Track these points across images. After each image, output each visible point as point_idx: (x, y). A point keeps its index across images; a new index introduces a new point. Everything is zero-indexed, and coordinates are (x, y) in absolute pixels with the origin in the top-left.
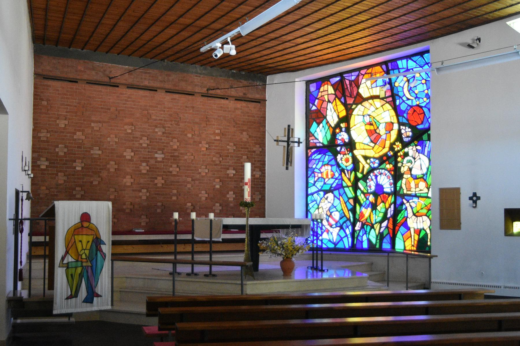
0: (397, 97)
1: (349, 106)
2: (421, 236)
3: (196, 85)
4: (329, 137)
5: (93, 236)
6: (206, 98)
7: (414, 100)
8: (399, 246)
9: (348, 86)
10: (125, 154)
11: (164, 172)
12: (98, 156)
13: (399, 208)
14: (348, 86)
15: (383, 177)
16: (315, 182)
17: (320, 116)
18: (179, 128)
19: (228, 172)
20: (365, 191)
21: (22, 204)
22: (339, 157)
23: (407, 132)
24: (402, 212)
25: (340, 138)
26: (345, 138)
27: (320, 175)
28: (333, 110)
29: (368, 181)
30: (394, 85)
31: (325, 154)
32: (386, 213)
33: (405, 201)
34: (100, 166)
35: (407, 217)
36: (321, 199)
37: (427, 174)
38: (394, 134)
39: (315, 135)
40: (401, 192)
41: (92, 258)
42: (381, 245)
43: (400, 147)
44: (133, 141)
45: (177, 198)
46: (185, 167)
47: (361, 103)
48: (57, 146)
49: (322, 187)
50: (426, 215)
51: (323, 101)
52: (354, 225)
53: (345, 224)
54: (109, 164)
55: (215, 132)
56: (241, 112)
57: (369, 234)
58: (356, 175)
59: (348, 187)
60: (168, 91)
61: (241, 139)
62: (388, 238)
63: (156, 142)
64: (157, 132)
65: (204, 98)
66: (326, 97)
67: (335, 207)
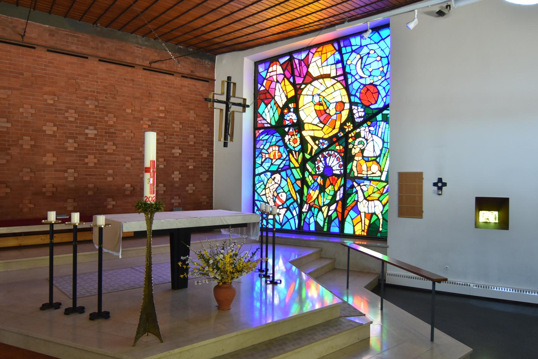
0: (349, 76)
2: (372, 221)
4: (277, 118)
6: (148, 72)
8: (348, 229)
9: (298, 65)
10: (44, 128)
11: (97, 150)
12: (5, 130)
13: (349, 192)
14: (298, 65)
16: (262, 163)
17: (268, 96)
19: (173, 151)
20: (313, 173)
22: (287, 138)
23: (359, 113)
24: (352, 196)
25: (288, 119)
26: (293, 118)
27: (267, 156)
28: (281, 91)
29: (316, 163)
30: (346, 64)
31: (272, 135)
32: (334, 196)
33: (355, 184)
34: (9, 141)
35: (358, 201)
36: (268, 180)
37: (380, 156)
38: (345, 114)
39: (264, 115)
42: (329, 228)
43: (352, 128)
44: (56, 113)
45: (113, 179)
47: (310, 83)
49: (270, 167)
50: (378, 200)
51: (272, 81)
52: (301, 207)
53: (292, 205)
56: (188, 90)
58: (304, 155)
59: (295, 168)
61: (188, 118)
62: (337, 221)
63: (87, 116)
64: (88, 105)
65: (145, 71)
66: (275, 77)
67: (282, 188)
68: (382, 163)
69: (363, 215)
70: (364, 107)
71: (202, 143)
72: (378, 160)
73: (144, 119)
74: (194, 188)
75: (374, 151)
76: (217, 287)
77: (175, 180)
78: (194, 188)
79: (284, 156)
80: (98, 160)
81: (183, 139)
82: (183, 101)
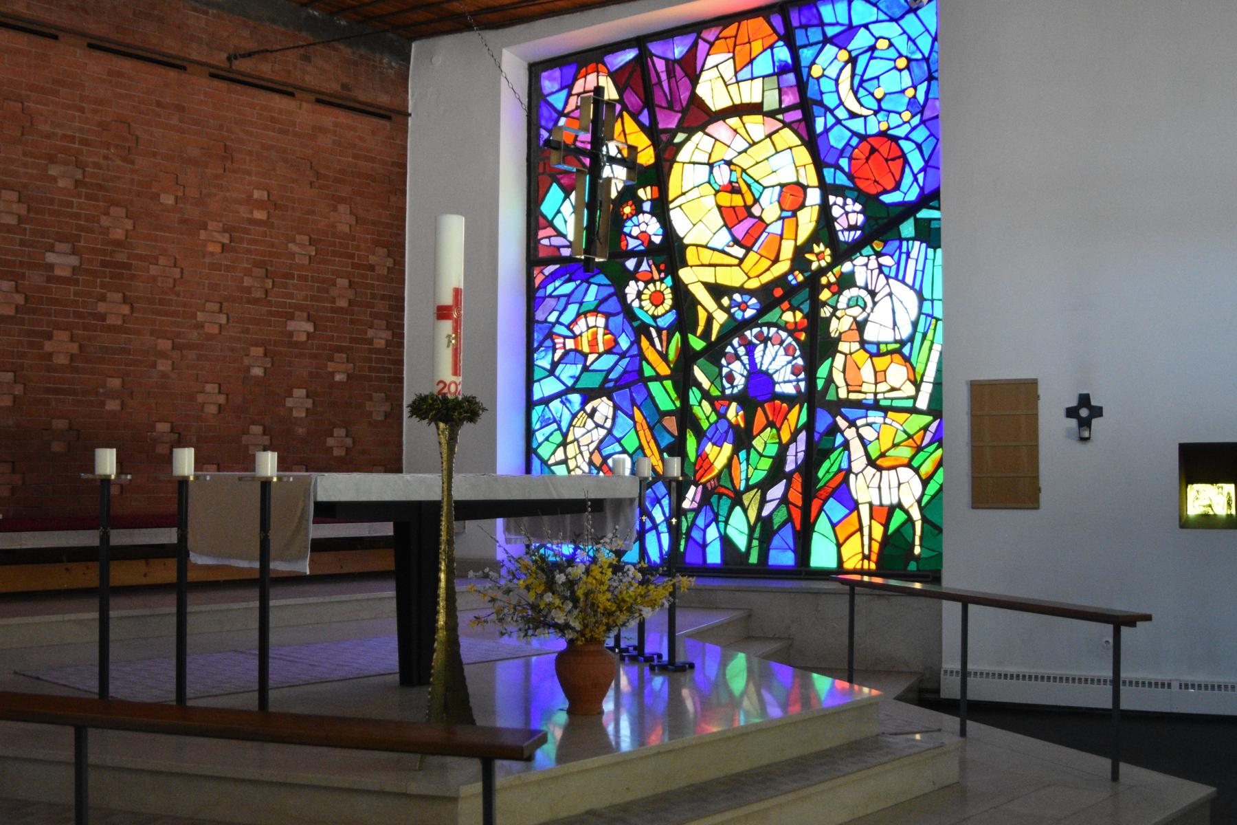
0: (817, 110)
1: (664, 137)
2: (893, 527)
6: (223, 85)
7: (872, 120)
8: (822, 555)
9: (664, 76)
11: (77, 315)
13: (825, 444)
14: (664, 76)
15: (771, 349)
16: (555, 365)
19: (292, 326)
20: (715, 392)
22: (632, 289)
23: (849, 215)
24: (833, 457)
25: (635, 232)
29: (724, 362)
30: (809, 75)
32: (780, 459)
36: (574, 416)
37: (911, 339)
38: (807, 220)
39: (558, 222)
40: (831, 396)
42: (764, 555)
43: (828, 259)
45: (123, 405)
47: (702, 128)
50: (909, 465)
55: (250, 196)
57: (726, 523)
58: (685, 341)
59: (658, 378)
60: (97, 46)
62: (787, 533)
64: (54, 179)
65: (216, 83)
67: (619, 440)
68: (918, 361)
69: (864, 511)
70: (863, 199)
71: (369, 305)
72: (906, 350)
73: (212, 225)
74: (349, 441)
75: (895, 324)
76: (562, 658)
77: (295, 414)
78: (349, 441)
79: (624, 342)
80: (81, 347)
81: (319, 290)
82: (318, 176)
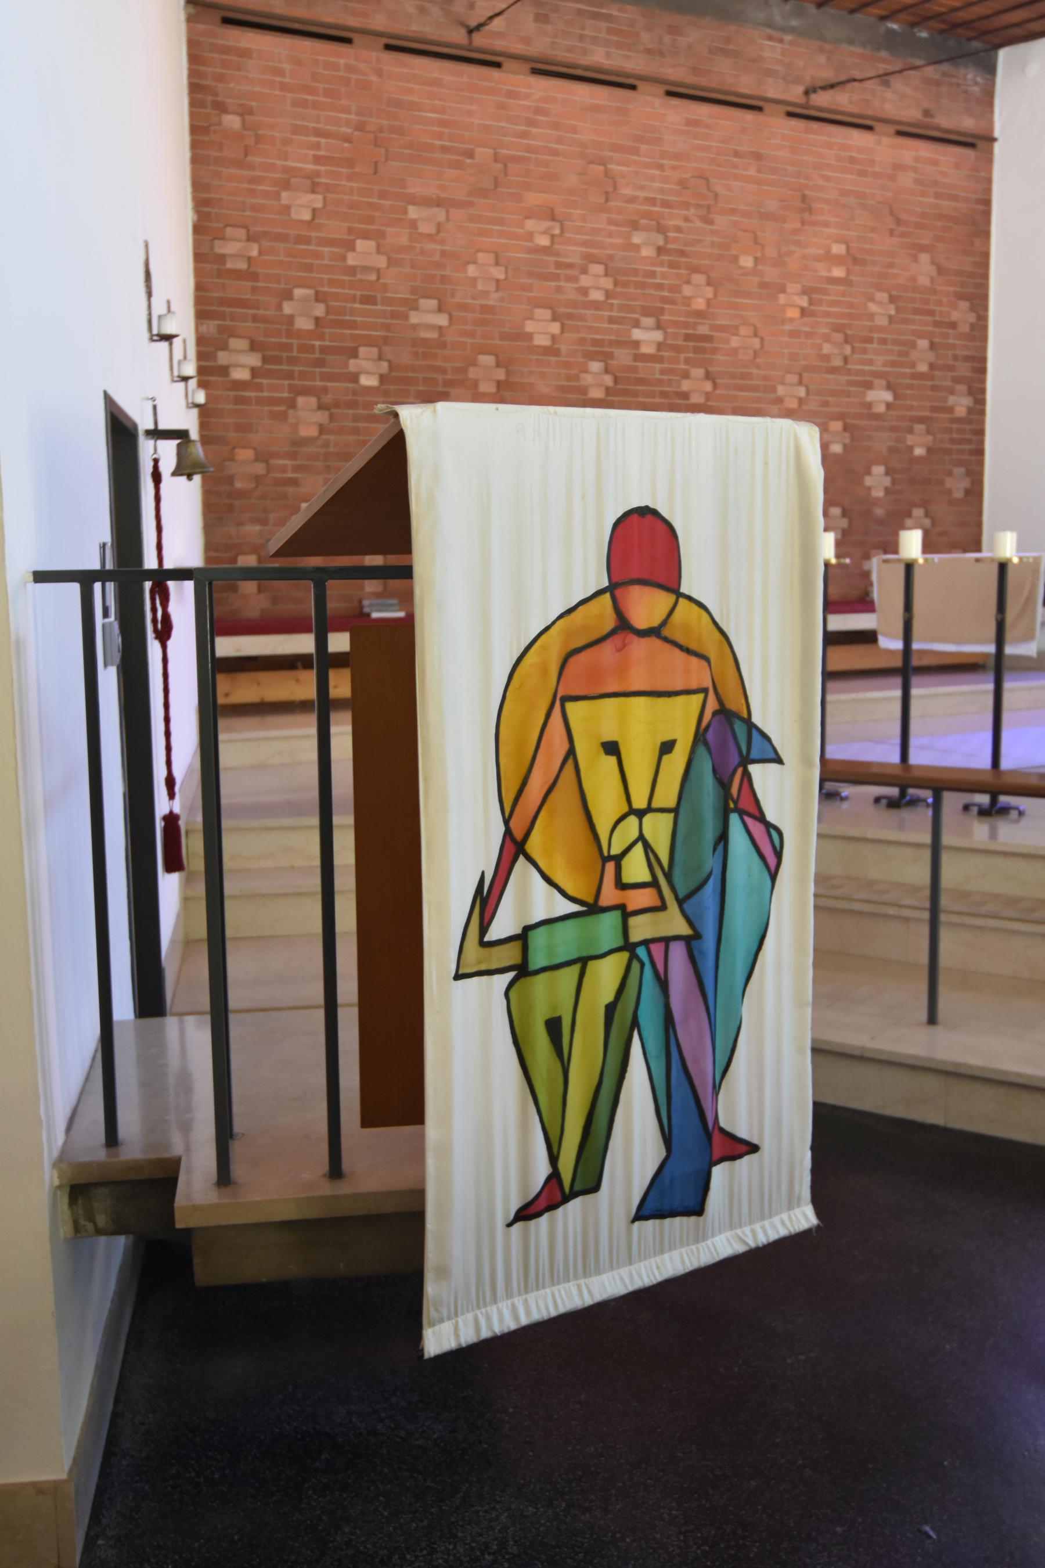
3: (769, 73)
5: (696, 700)
10: (529, 327)
18: (713, 233)
21: (158, 499)
41: (694, 882)
44: (556, 277)
46: (733, 376)
48: (288, 296)
54: (474, 364)
55: (828, 251)
61: (913, 279)
64: (637, 248)
65: (794, 122)
